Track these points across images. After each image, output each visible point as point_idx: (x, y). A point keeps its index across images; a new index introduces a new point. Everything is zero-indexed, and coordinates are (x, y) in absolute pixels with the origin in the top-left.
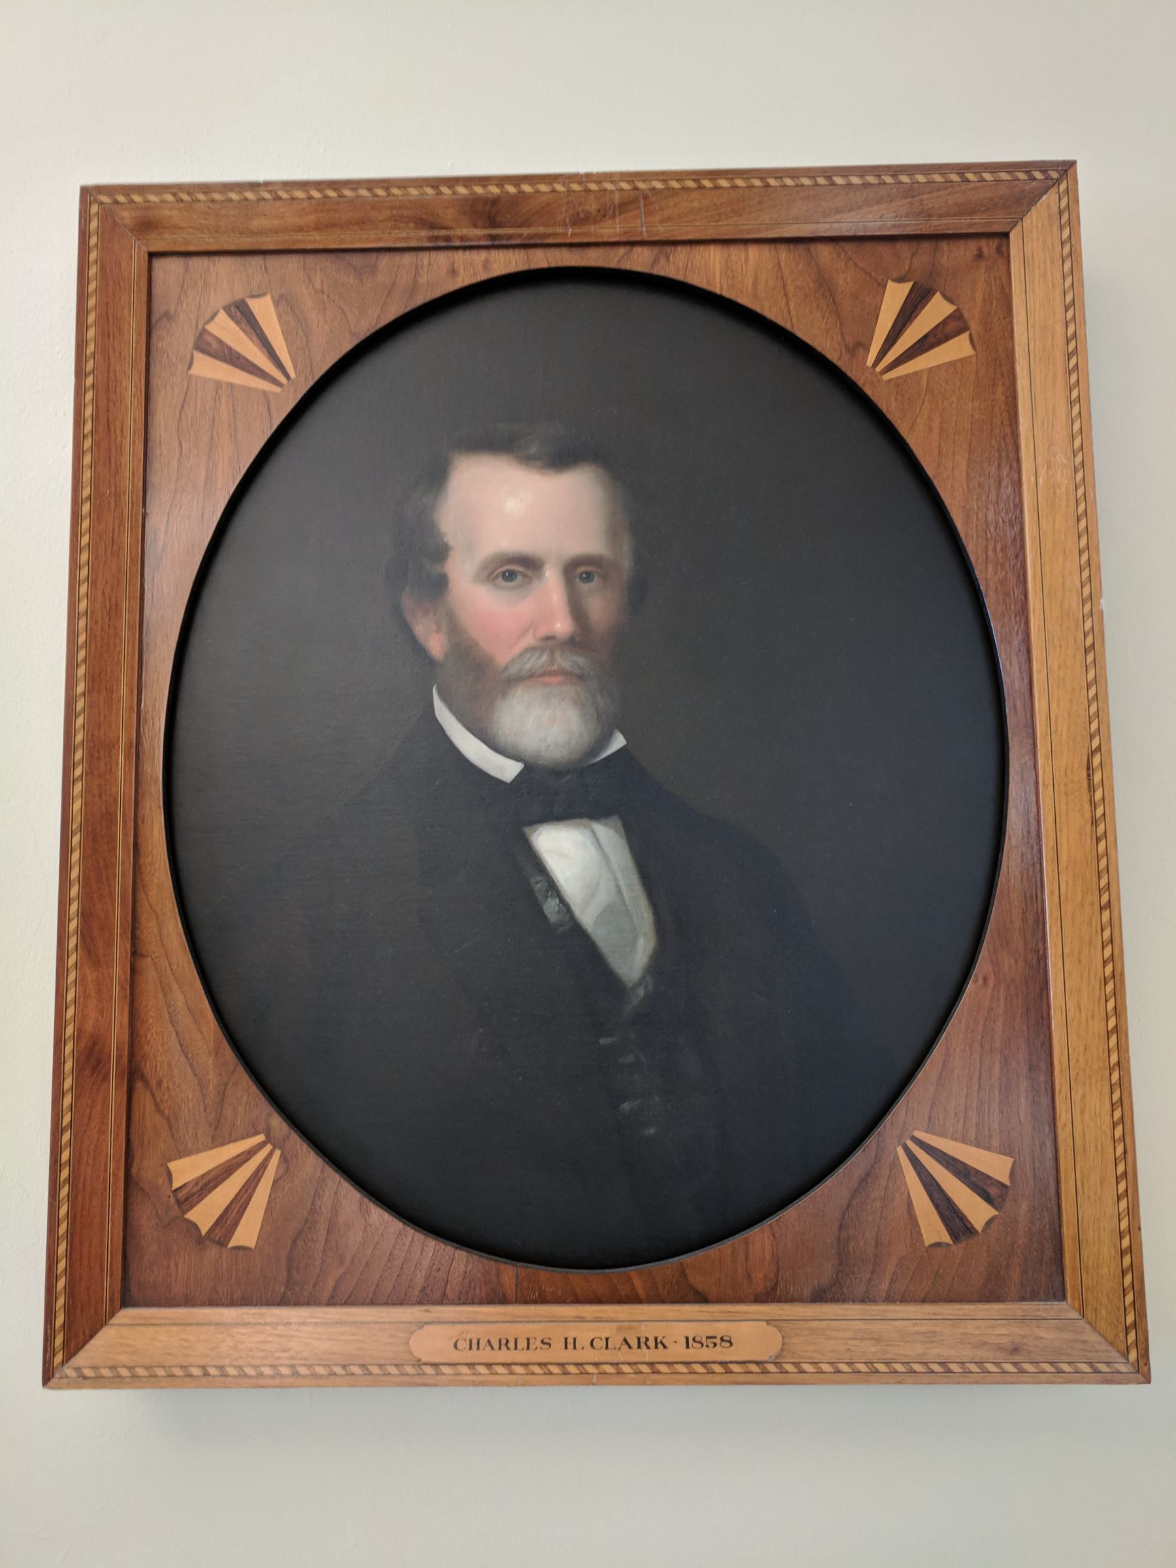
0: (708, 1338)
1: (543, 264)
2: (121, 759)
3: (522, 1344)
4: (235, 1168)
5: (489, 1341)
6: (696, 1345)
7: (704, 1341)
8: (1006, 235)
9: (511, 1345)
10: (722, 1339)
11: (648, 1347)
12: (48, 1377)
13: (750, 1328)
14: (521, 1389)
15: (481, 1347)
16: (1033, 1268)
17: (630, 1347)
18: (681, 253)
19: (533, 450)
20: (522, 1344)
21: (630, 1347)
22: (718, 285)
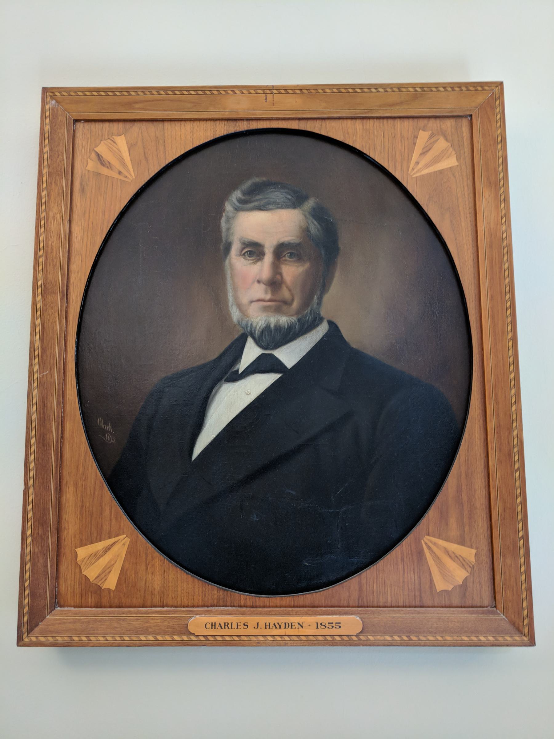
0: (329, 623)
1: (265, 127)
2: (228, 374)
3: (234, 626)
4: (110, 552)
5: (220, 624)
6: (323, 627)
7: (327, 625)
9: (230, 626)
10: (321, 624)
12: (20, 642)
13: (351, 623)
14: (349, 647)
15: (271, 627)
17: (221, 628)
18: (334, 123)
19: (323, 224)
20: (234, 626)
22: (316, 131)
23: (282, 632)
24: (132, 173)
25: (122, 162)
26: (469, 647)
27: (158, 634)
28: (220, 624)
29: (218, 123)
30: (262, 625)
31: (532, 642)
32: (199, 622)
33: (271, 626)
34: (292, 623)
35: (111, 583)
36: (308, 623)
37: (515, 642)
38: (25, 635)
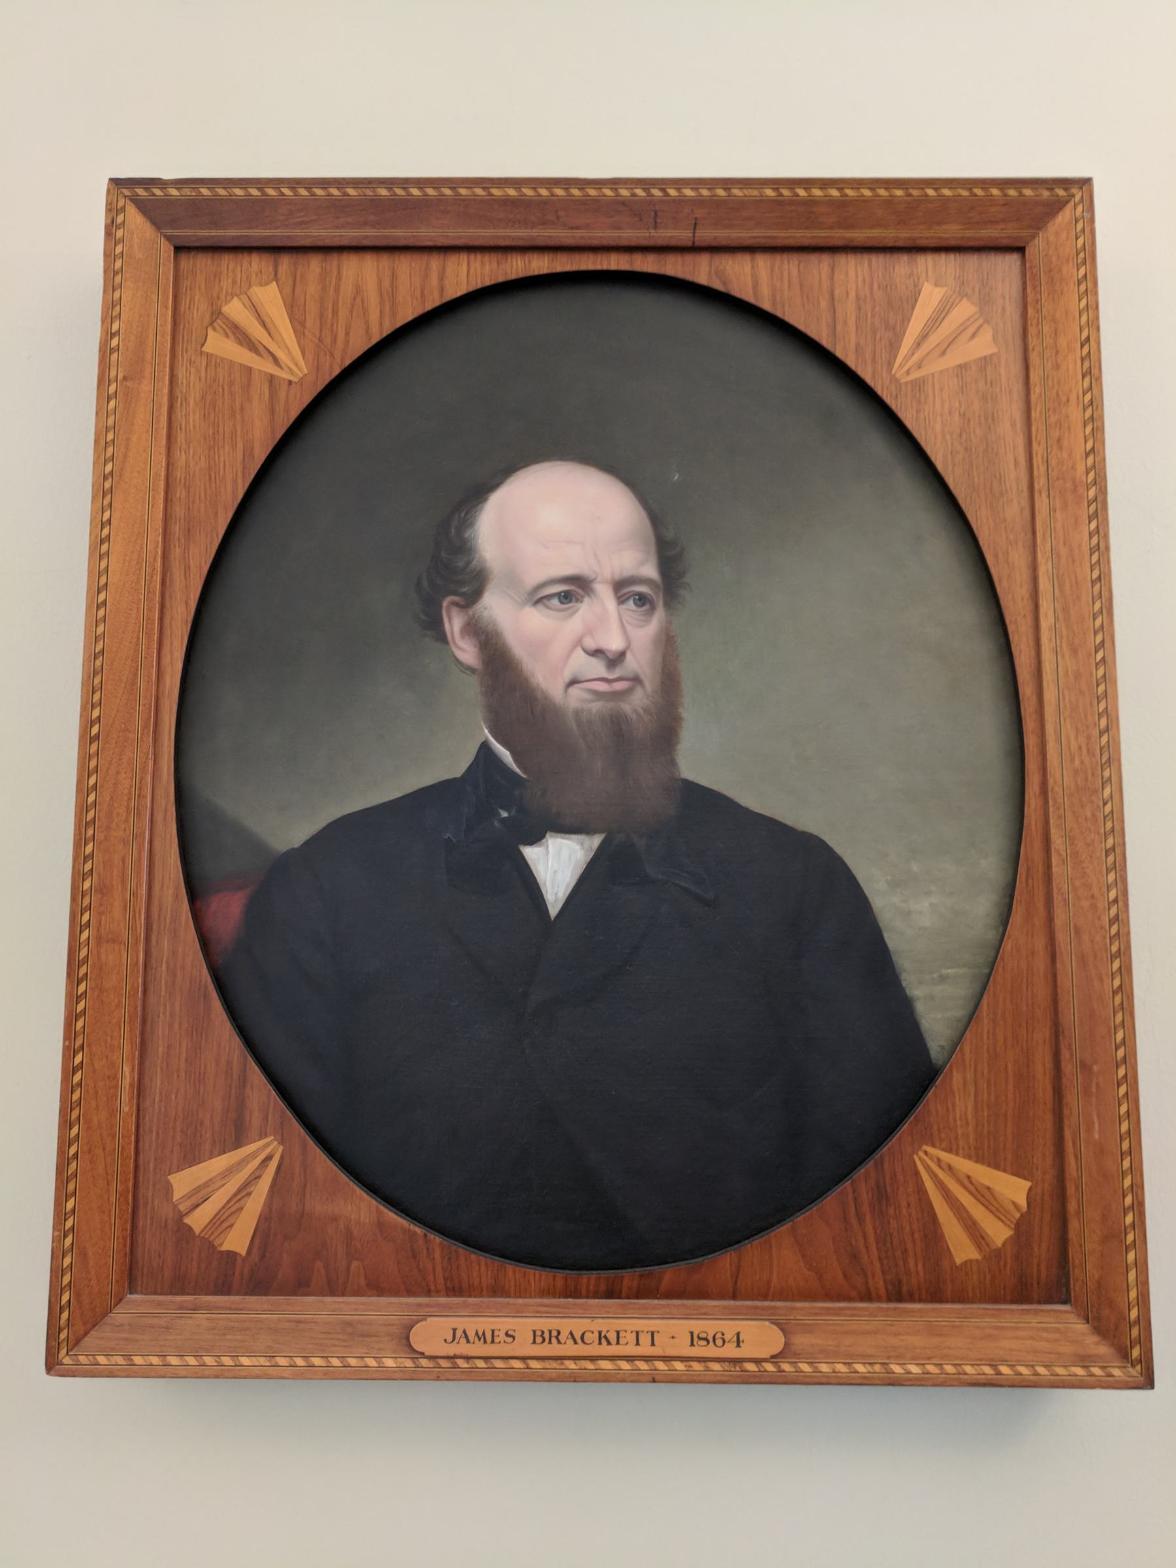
1: (591, 267)
3: (612, 1337)
5: (464, 1332)
8: (1021, 250)
9: (489, 1339)
11: (559, 1342)
13: (758, 1337)
16: (1061, 1281)
17: (468, 1341)
21: (468, 1341)
23: (478, 1349)
24: (302, 363)
25: (275, 335)
26: (1010, 1390)
27: (929, 1358)
28: (464, 1332)
29: (813, 258)
30: (645, 1339)
31: (1148, 1382)
32: (435, 1332)
33: (562, 1338)
34: (493, 1331)
35: (237, 1240)
36: (668, 1328)
37: (1110, 1379)
38: (63, 1352)
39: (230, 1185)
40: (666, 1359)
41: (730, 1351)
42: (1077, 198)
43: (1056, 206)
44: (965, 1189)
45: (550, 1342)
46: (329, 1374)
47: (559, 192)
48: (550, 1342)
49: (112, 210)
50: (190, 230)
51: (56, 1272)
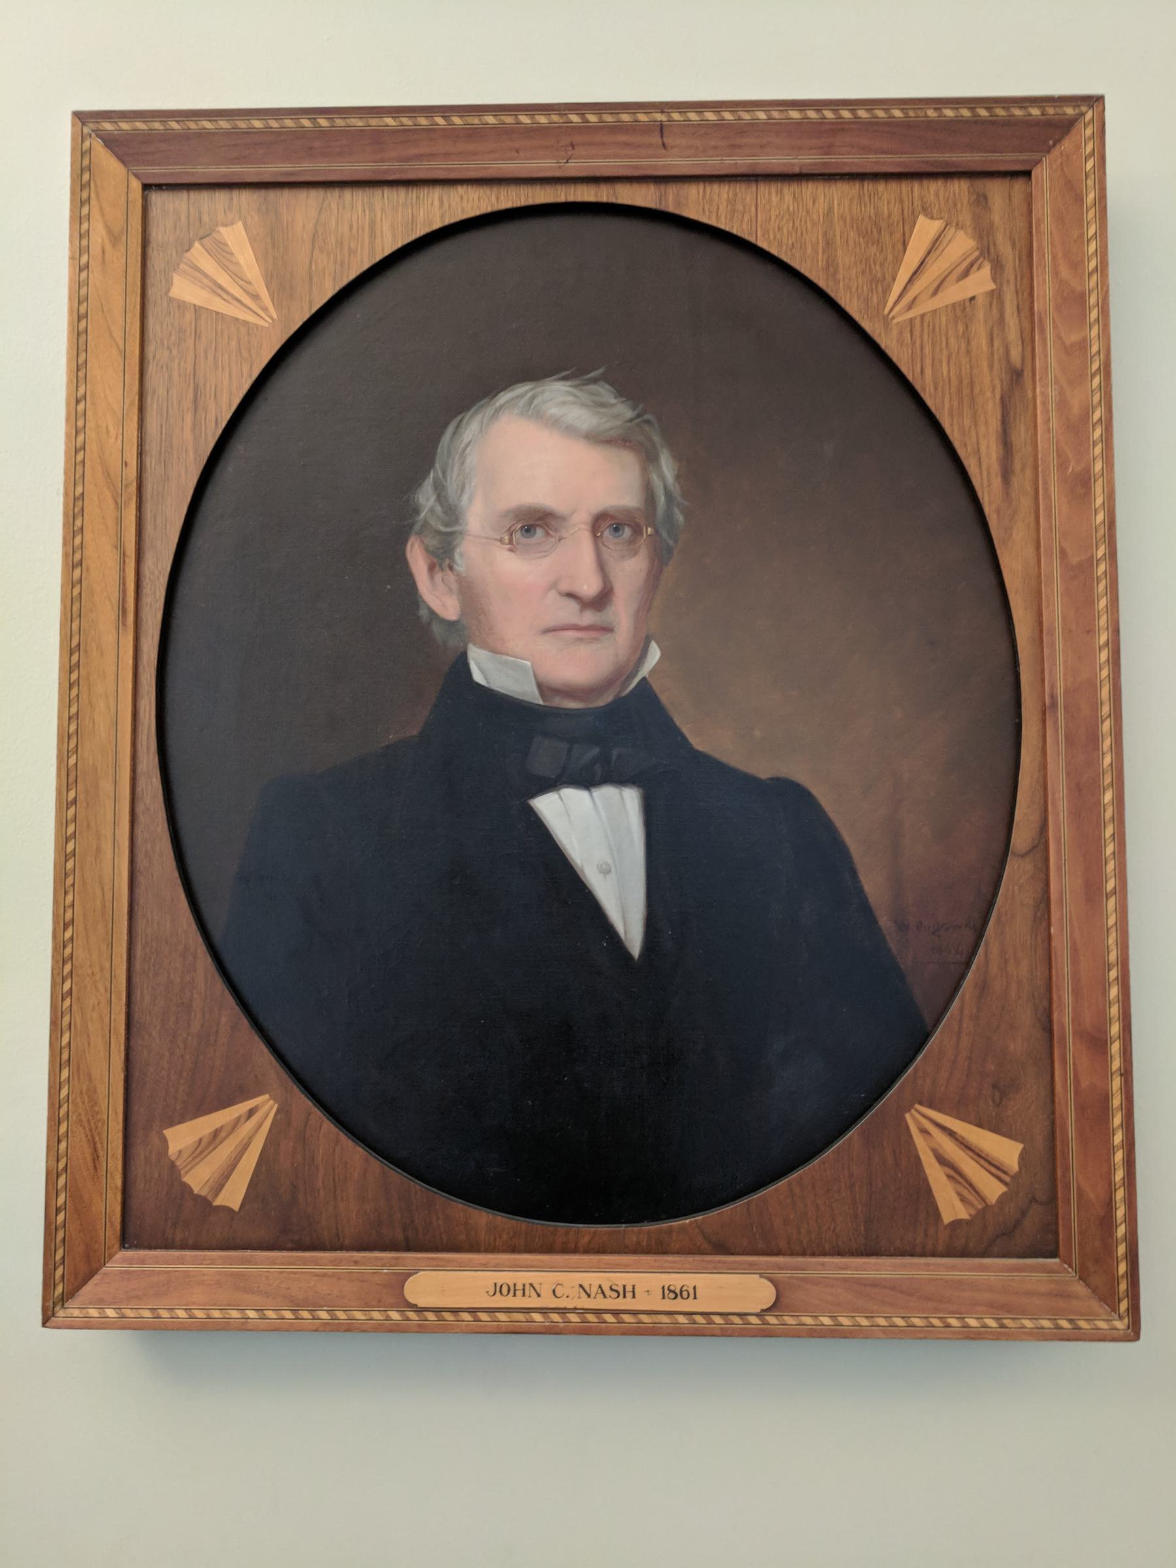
8: (1027, 174)
13: (739, 1288)
16: (1059, 1244)
25: (240, 281)
32: (437, 1283)
39: (224, 1147)
40: (562, 1311)
41: (548, 1301)
42: (1089, 116)
43: (1066, 126)
44: (962, 1157)
45: (515, 1295)
46: (892, 1332)
47: (812, 114)
48: (515, 1295)
49: (79, 140)
50: (153, 164)
51: (50, 1229)
